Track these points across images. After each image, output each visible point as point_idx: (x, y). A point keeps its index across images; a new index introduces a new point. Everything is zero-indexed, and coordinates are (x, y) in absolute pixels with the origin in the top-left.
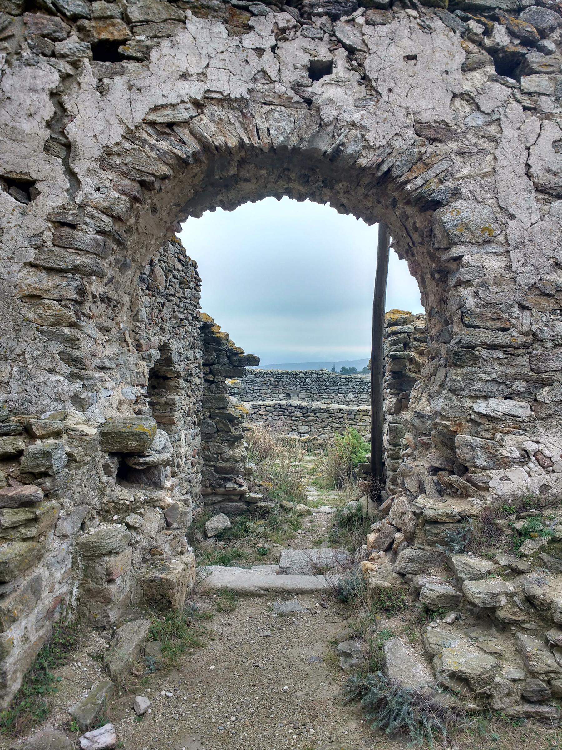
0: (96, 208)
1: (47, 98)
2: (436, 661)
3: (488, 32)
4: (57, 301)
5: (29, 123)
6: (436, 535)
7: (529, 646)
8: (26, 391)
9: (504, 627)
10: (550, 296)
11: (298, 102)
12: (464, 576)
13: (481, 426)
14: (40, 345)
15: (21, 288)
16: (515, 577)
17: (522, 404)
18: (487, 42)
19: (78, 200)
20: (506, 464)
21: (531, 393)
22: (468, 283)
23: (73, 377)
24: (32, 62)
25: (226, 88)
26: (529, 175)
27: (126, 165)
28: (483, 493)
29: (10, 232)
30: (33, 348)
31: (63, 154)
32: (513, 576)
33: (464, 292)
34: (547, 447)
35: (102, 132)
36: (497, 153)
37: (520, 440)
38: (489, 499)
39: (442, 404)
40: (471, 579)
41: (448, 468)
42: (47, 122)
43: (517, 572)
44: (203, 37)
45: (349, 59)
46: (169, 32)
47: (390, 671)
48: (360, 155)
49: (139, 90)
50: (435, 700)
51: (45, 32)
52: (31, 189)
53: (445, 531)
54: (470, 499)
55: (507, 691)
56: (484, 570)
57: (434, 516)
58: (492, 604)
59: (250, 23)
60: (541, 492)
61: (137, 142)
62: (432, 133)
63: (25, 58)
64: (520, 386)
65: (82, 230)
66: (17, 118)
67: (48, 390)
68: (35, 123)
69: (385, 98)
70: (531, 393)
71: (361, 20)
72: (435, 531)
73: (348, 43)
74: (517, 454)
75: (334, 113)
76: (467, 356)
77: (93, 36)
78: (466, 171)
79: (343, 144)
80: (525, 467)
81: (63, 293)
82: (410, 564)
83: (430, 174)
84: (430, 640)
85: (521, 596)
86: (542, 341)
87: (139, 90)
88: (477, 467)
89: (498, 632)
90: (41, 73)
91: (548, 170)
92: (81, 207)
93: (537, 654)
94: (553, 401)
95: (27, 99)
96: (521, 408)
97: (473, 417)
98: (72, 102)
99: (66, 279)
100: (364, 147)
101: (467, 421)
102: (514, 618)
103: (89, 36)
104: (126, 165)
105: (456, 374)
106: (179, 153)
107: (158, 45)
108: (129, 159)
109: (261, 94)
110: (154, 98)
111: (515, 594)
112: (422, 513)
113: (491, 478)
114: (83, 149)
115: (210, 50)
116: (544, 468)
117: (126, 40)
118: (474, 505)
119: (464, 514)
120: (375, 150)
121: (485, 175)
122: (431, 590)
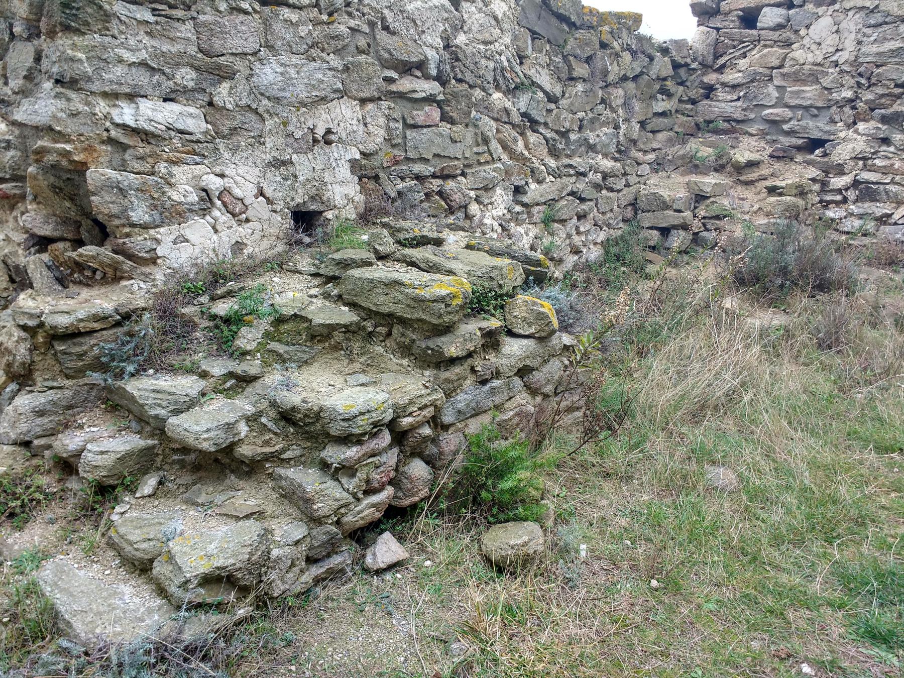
2: (160, 569)
6: (80, 356)
7: (308, 484)
9: (250, 469)
12: (162, 412)
13: (130, 151)
16: (244, 389)
17: (192, 110)
20: (180, 214)
21: (204, 90)
28: (147, 270)
32: (241, 387)
34: (236, 183)
37: (197, 172)
38: (159, 277)
39: (53, 109)
40: (177, 412)
43: (245, 380)
47: (79, 626)
50: (188, 636)
53: (93, 347)
54: (124, 283)
55: (290, 562)
56: (193, 393)
57: (72, 324)
58: (228, 441)
60: (234, 253)
64: (186, 76)
70: (204, 90)
74: (193, 198)
76: (90, 10)
80: (208, 217)
82: (39, 421)
84: (132, 538)
85: (273, 414)
88: (133, 225)
89: (241, 479)
93: (322, 491)
94: (237, 105)
96: (187, 117)
97: (113, 133)
101: (103, 142)
102: (267, 450)
105: (74, 46)
111: (259, 414)
112: (41, 325)
113: (158, 242)
116: (234, 215)
118: (136, 292)
119: (123, 310)
122: (102, 453)
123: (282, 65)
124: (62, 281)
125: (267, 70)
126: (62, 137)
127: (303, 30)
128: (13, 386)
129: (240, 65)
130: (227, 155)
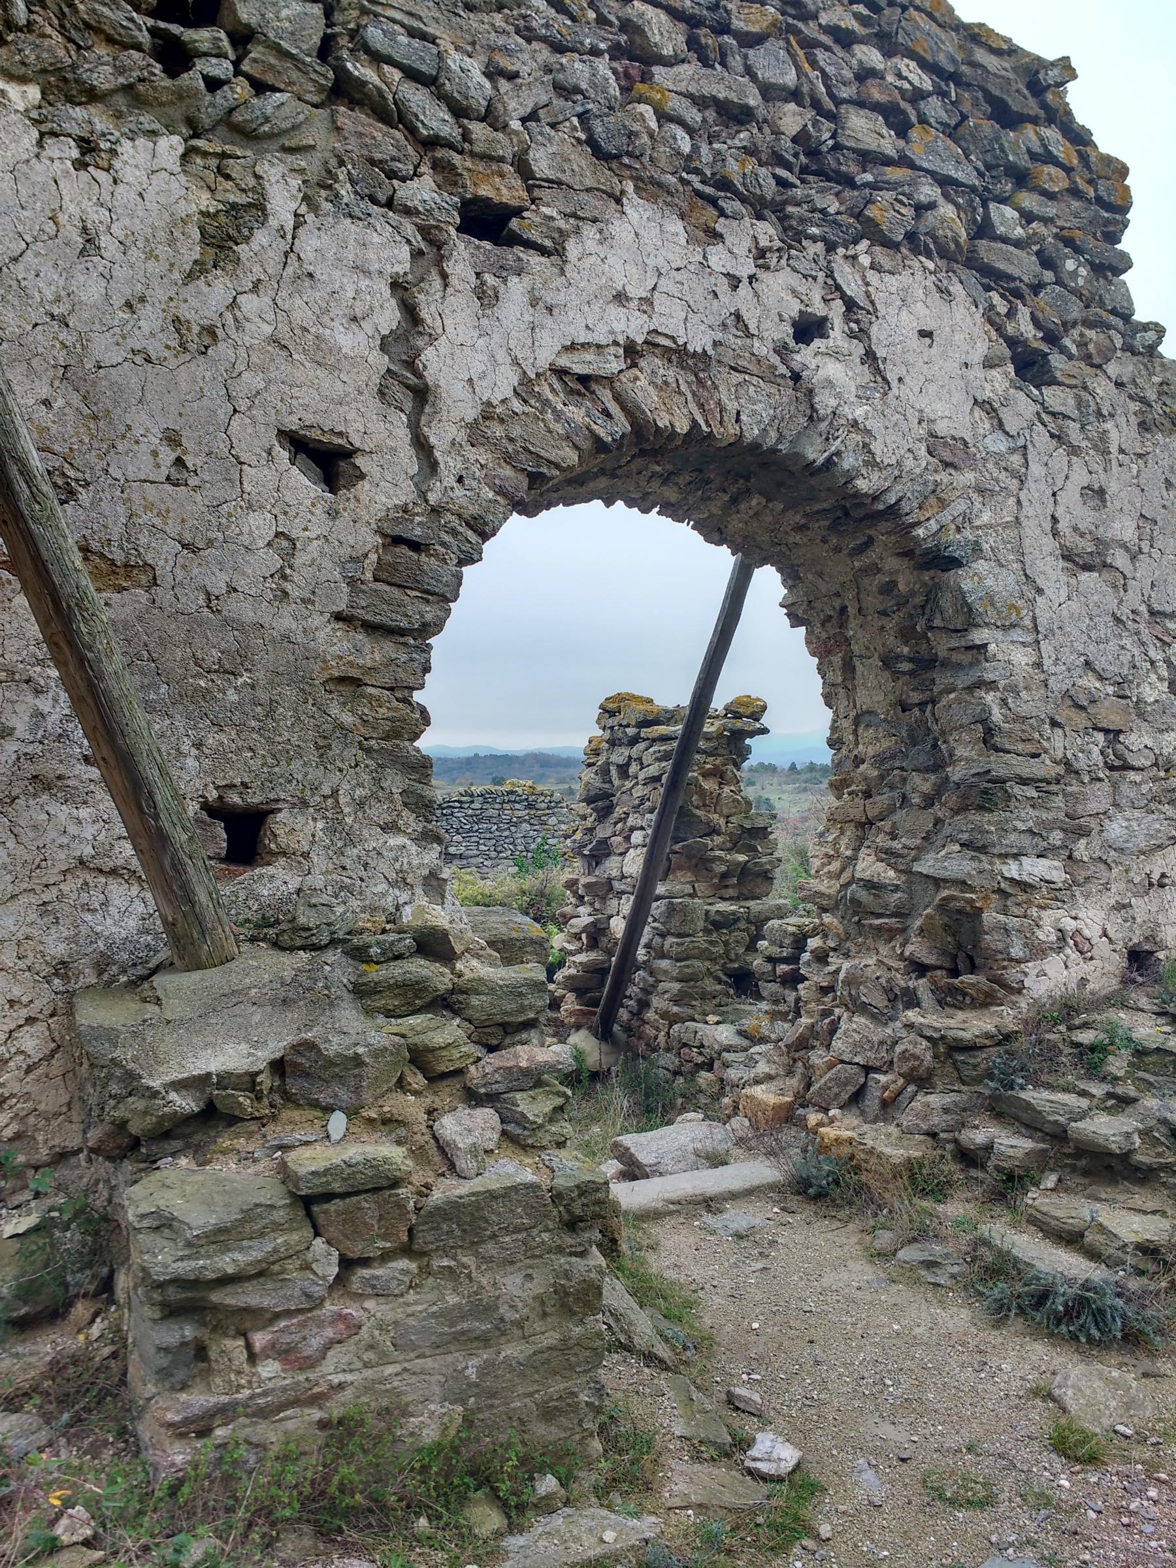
0: (460, 516)
1: (387, 292)
3: (1011, 314)
4: (391, 689)
8: (344, 868)
10: (1082, 708)
11: (783, 376)
13: (1012, 899)
15: (325, 661)
17: (1056, 863)
18: (1010, 329)
19: (433, 498)
22: (991, 685)
23: (427, 838)
25: (682, 332)
26: (1055, 534)
27: (511, 440)
28: (1013, 998)
29: (309, 549)
31: (408, 405)
33: (990, 698)
35: (483, 376)
36: (1022, 495)
41: (947, 965)
42: (383, 338)
44: (651, 235)
45: (847, 319)
46: (596, 213)
48: (859, 475)
49: (550, 309)
51: (378, 156)
52: (342, 464)
59: (719, 228)
62: (947, 452)
63: (345, 200)
65: (436, 556)
66: (325, 319)
67: (383, 866)
69: (895, 391)
71: (865, 260)
72: (972, 1061)
73: (849, 293)
74: (1053, 938)
75: (833, 402)
77: (464, 187)
78: (986, 517)
79: (838, 453)
81: (401, 675)
83: (946, 517)
86: (1077, 773)
88: (1011, 960)
90: (376, 239)
91: (1075, 529)
92: (436, 511)
95: (349, 285)
98: (433, 309)
99: (402, 649)
100: (866, 464)
103: (455, 184)
104: (511, 440)
106: (601, 433)
107: (577, 231)
108: (516, 431)
109: (57, 206)
110: (571, 329)
113: (1026, 974)
114: (449, 402)
115: (660, 262)
116: (1081, 953)
118: (1006, 1017)
120: (880, 470)
121: (1006, 526)
123: (1128, 820)
124: (941, 1003)
125: (1115, 825)
126: (972, 889)
127: (1145, 788)
128: (911, 1088)
129: (1093, 824)
130: (1081, 900)
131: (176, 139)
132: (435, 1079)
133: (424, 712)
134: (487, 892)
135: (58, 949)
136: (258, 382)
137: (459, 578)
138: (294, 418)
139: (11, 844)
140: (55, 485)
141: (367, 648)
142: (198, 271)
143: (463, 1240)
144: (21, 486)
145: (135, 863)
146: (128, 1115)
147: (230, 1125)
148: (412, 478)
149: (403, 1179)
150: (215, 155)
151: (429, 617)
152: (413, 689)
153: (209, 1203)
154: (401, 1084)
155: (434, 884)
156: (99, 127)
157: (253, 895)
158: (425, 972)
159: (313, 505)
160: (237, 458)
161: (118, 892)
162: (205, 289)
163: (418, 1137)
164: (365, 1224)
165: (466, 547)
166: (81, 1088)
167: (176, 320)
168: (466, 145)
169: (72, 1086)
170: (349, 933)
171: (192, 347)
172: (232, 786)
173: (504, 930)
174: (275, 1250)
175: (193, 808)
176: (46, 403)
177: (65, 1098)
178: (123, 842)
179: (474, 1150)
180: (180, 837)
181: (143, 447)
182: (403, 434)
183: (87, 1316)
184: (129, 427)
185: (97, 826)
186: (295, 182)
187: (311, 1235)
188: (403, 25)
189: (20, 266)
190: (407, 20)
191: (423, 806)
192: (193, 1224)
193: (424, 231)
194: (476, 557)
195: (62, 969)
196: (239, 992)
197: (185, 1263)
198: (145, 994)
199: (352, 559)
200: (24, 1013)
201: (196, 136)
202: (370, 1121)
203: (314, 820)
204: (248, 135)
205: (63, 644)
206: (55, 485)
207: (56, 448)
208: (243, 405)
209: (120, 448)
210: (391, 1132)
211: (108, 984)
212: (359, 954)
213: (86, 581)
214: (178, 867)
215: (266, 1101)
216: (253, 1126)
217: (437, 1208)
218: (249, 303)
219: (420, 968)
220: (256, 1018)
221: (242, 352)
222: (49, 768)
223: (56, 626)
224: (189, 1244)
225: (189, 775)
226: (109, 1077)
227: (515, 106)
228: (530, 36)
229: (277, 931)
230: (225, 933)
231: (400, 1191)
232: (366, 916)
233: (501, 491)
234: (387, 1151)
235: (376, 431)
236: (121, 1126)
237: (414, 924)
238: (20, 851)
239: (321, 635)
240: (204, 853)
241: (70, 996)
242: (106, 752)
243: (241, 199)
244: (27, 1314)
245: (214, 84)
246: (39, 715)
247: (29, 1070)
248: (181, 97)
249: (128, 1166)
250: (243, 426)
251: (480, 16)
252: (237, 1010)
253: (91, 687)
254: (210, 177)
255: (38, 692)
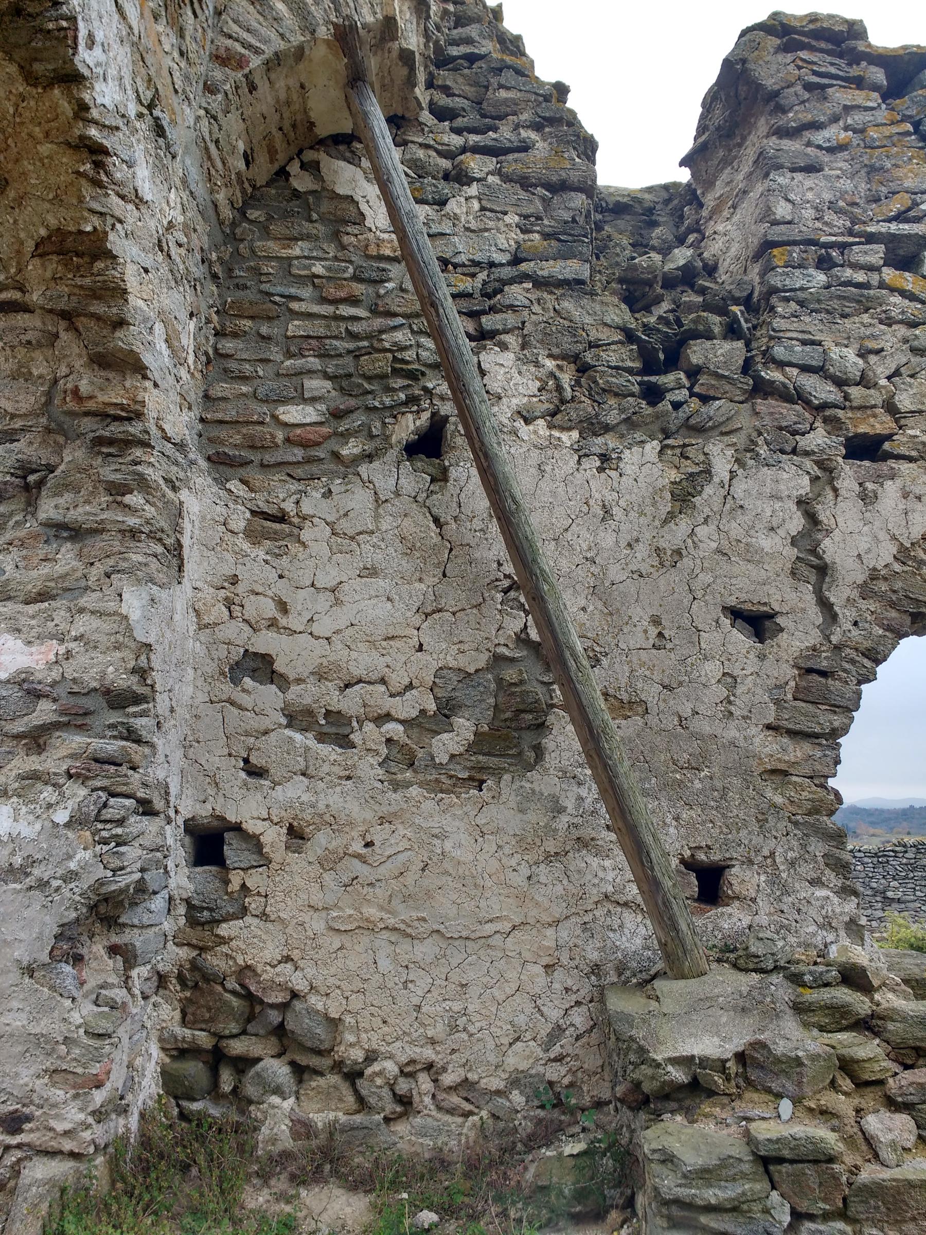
0: (857, 650)
4: (811, 777)
5: (770, 540)
8: (782, 912)
14: (795, 843)
15: (760, 759)
19: (835, 639)
23: (847, 891)
24: (771, 461)
27: (894, 592)
30: (786, 847)
31: (813, 579)
35: (869, 551)
49: (919, 498)
51: (784, 424)
52: (768, 624)
61: (910, 563)
66: (752, 532)
67: (813, 912)
68: (777, 539)
77: (847, 429)
87: (919, 498)
90: (785, 476)
92: (837, 648)
98: (828, 513)
103: (841, 429)
108: (898, 585)
114: (843, 572)
117: (892, 435)
131: (655, 442)
132: (861, 1085)
133: (837, 794)
134: (919, 936)
135: (594, 956)
136: (708, 578)
137: (859, 695)
138: (733, 598)
139: (565, 882)
140: (589, 657)
141: (791, 748)
142: (671, 517)
143: (888, 1216)
144: (572, 663)
145: (639, 899)
146: (642, 1078)
147: (709, 1097)
148: (818, 627)
149: (836, 1157)
150: (679, 446)
151: (836, 724)
152: (828, 777)
153: (696, 1149)
154: (833, 1084)
155: (854, 928)
156: (611, 446)
157: (717, 927)
158: (848, 999)
159: (748, 652)
160: (696, 628)
161: (631, 919)
162: (674, 528)
163: (848, 1128)
164: (810, 1187)
165: (863, 671)
166: (610, 1057)
167: (658, 549)
168: (847, 403)
169: (604, 1054)
170: (788, 962)
171: (667, 564)
172: (700, 848)
173: (916, 970)
174: (744, 1194)
175: (675, 862)
176: (584, 609)
177: (600, 1063)
178: (631, 884)
179: (893, 1144)
180: (668, 883)
181: (639, 628)
182: (810, 598)
183: (620, 1220)
184: (630, 617)
185: (616, 872)
186: (730, 452)
187: (769, 1187)
188: (798, 340)
189: (569, 533)
190: (800, 336)
191: (842, 868)
192: (687, 1162)
193: (819, 464)
194: (871, 677)
195: (596, 969)
196: (711, 998)
197: (683, 1189)
198: (649, 993)
199: (777, 687)
200: (574, 998)
201: (667, 437)
202: (811, 1110)
203: (759, 874)
204: (700, 430)
205: (595, 756)
206: (589, 657)
207: (589, 635)
208: (699, 594)
209: (625, 631)
210: (827, 1121)
211: (625, 983)
212: (796, 979)
213: (607, 716)
214: (667, 904)
215: (733, 1083)
216: (726, 1100)
217: (865, 1186)
218: (702, 531)
219: (844, 995)
220: (724, 1019)
221: (698, 561)
222: (587, 833)
223: (591, 745)
224: (685, 1176)
225: (672, 841)
226: (629, 1048)
227: (881, 369)
228: (889, 322)
229: (736, 956)
230: (699, 954)
231: (834, 1166)
232: (801, 950)
233: (888, 628)
234: (822, 1133)
235: (793, 601)
236: (637, 1085)
237: (839, 960)
238: (570, 887)
239: (757, 740)
240: (683, 895)
241: (602, 989)
242: (620, 824)
243: (696, 469)
244: (580, 1212)
245: (677, 406)
246: (580, 799)
247: (577, 1038)
248: (658, 418)
249: (643, 1116)
250: (700, 608)
251: (852, 319)
252: (710, 1012)
253: (611, 781)
254: (676, 460)
255: (580, 784)
